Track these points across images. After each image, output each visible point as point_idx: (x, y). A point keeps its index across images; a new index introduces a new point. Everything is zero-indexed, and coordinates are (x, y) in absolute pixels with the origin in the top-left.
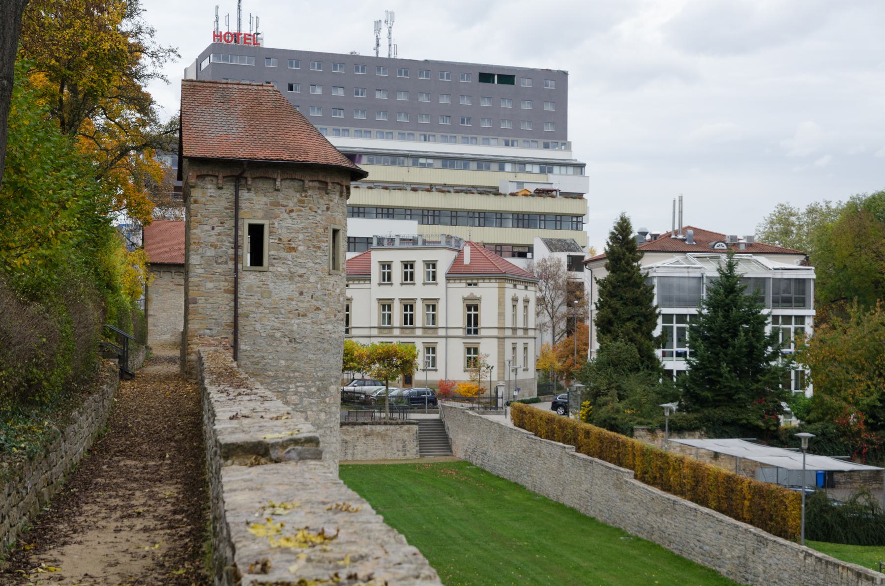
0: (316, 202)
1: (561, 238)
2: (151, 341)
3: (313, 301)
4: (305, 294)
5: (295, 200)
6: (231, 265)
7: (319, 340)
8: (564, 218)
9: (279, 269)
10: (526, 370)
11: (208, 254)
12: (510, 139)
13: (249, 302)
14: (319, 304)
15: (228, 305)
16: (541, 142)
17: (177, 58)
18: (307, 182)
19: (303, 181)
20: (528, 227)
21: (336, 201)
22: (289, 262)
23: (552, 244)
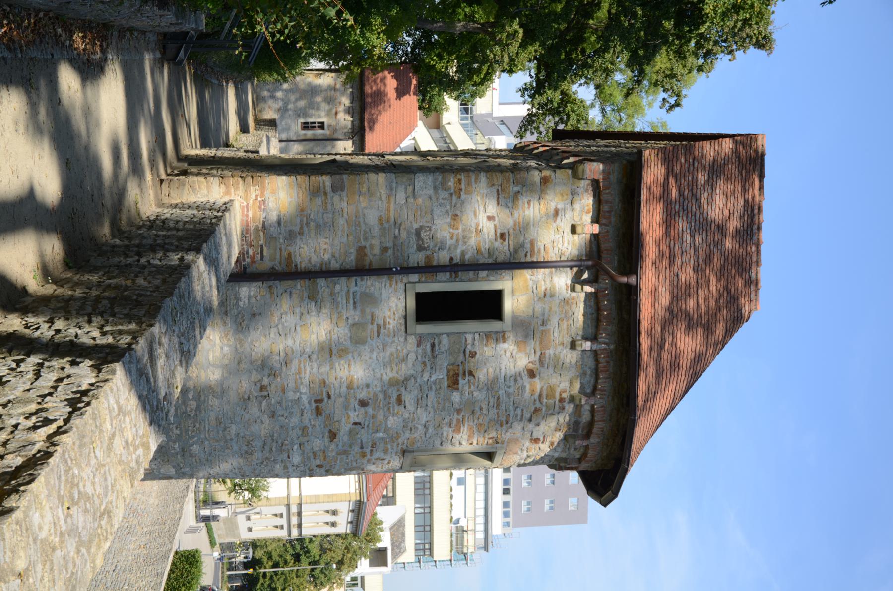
4: (362, 409)
7: (269, 441)
22: (426, 376)
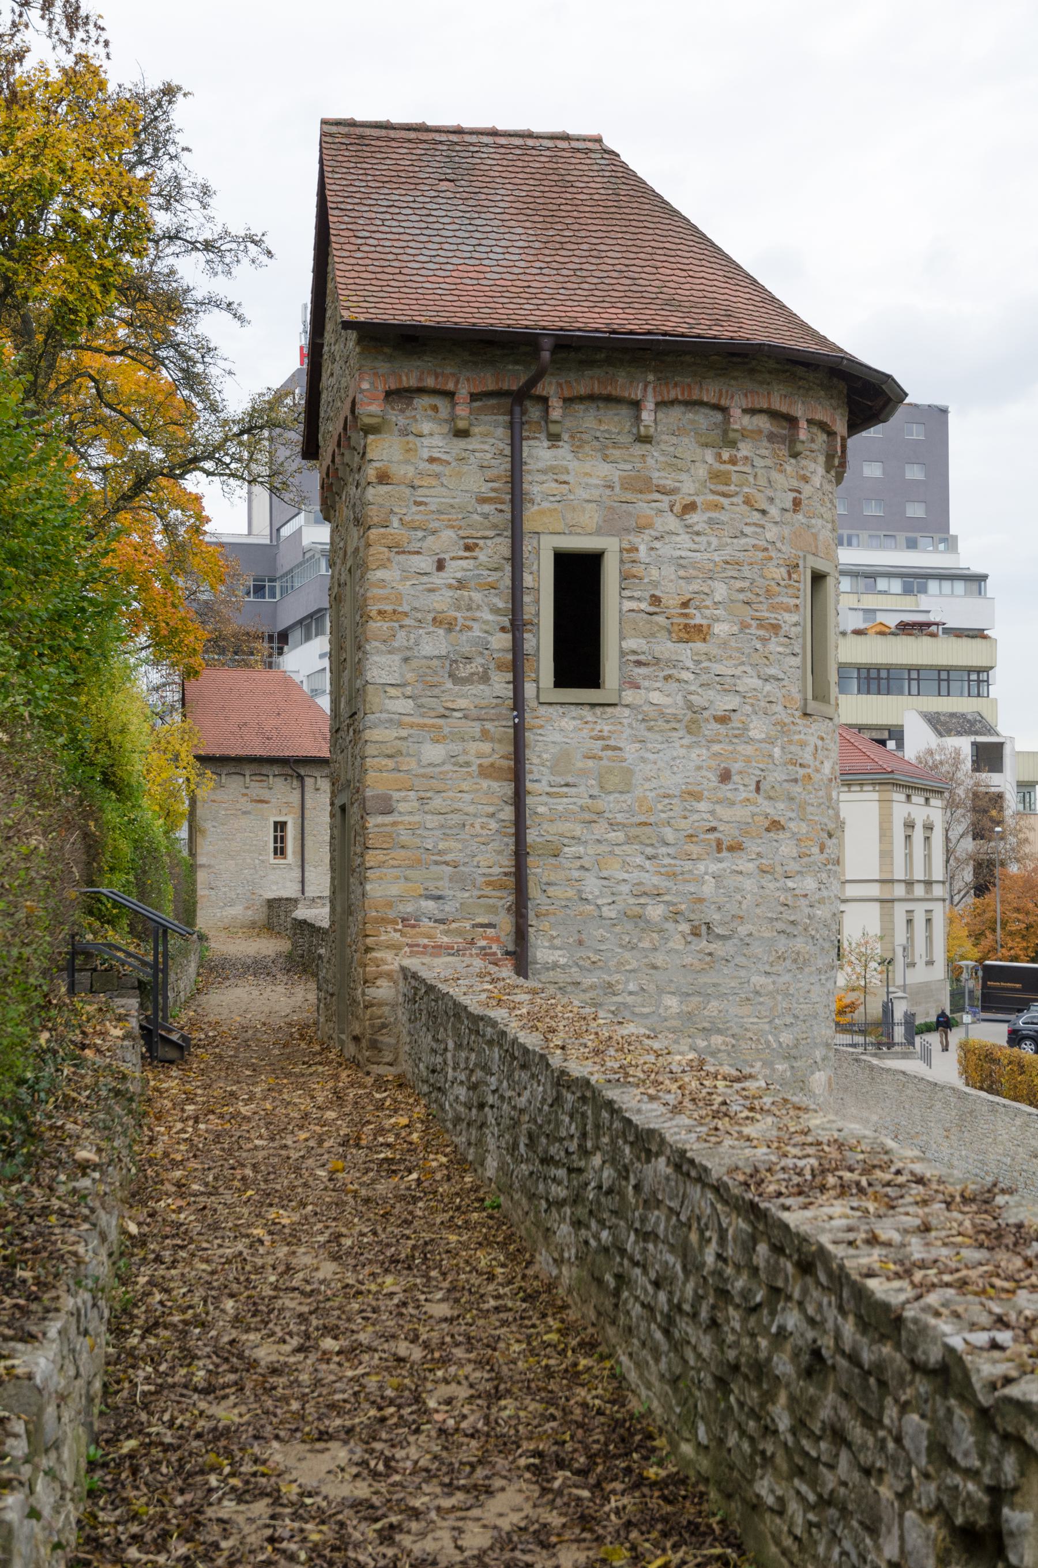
0: (762, 482)
1: (955, 710)
2: (204, 921)
3: (760, 800)
4: (736, 778)
5: (702, 472)
6: (501, 685)
7: (780, 926)
8: (953, 675)
9: (655, 697)
10: (930, 963)
11: (428, 648)
12: (845, 533)
13: (561, 805)
14: (778, 810)
15: (493, 815)
16: (902, 537)
17: (264, 258)
18: (736, 412)
19: (724, 410)
20: (888, 693)
21: (817, 481)
22: (686, 675)
23: (939, 721)
